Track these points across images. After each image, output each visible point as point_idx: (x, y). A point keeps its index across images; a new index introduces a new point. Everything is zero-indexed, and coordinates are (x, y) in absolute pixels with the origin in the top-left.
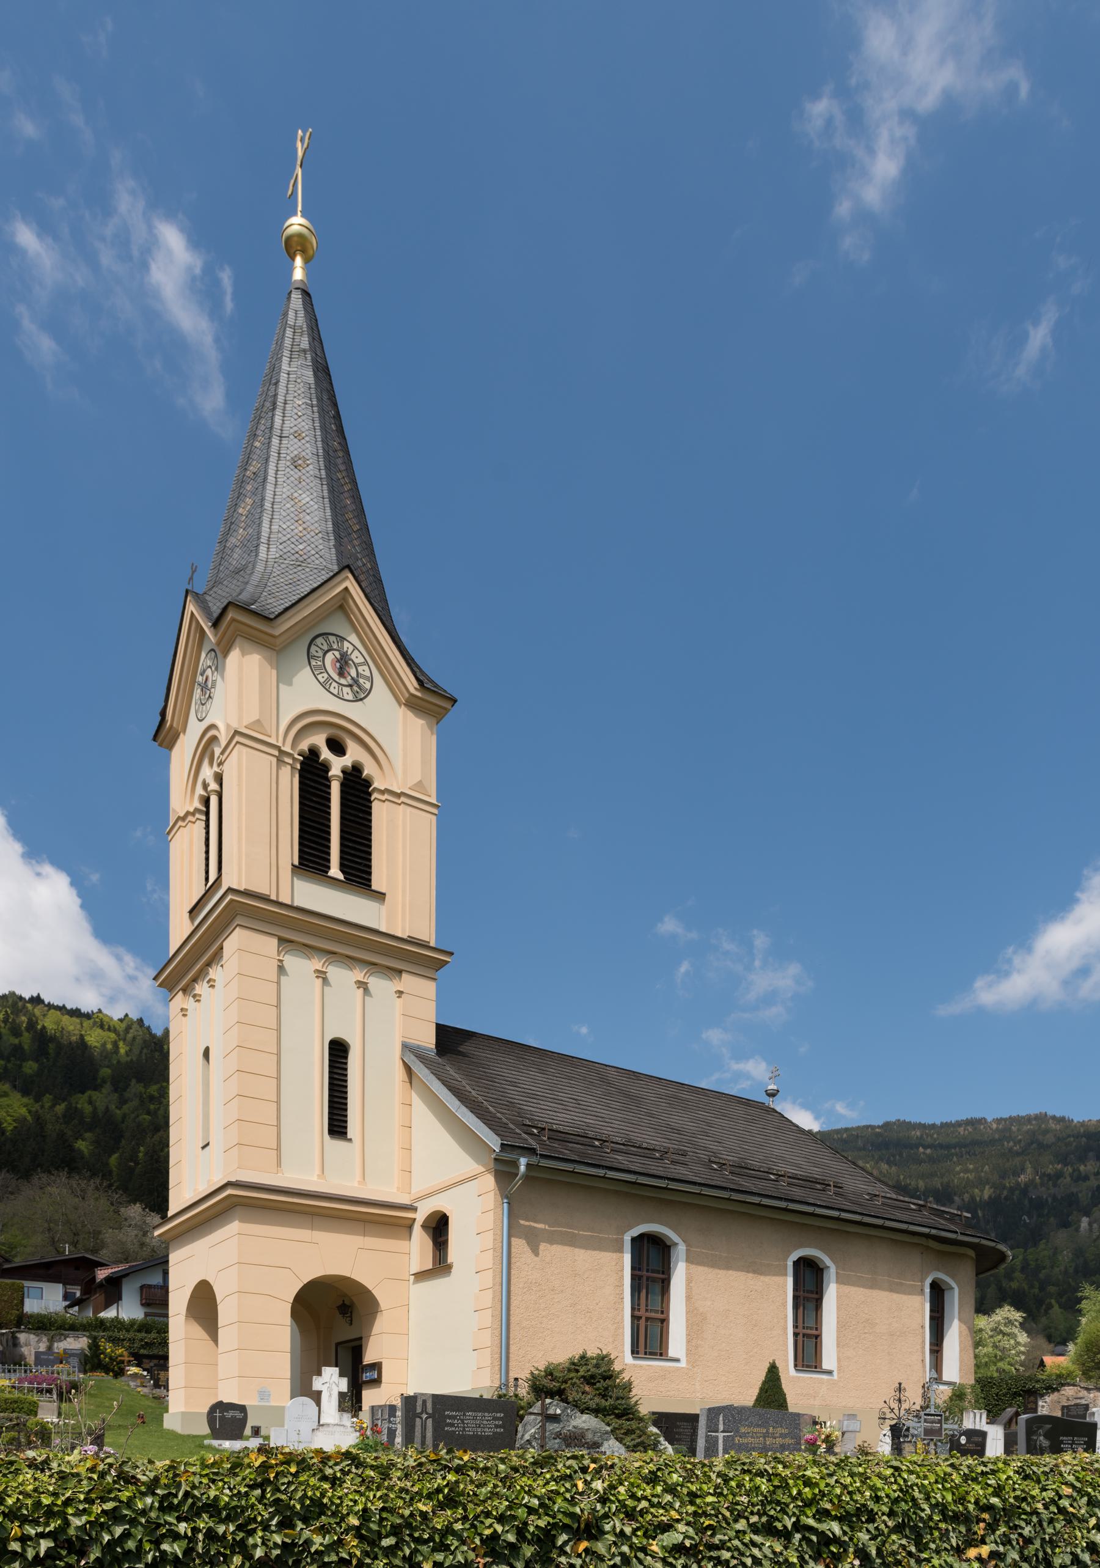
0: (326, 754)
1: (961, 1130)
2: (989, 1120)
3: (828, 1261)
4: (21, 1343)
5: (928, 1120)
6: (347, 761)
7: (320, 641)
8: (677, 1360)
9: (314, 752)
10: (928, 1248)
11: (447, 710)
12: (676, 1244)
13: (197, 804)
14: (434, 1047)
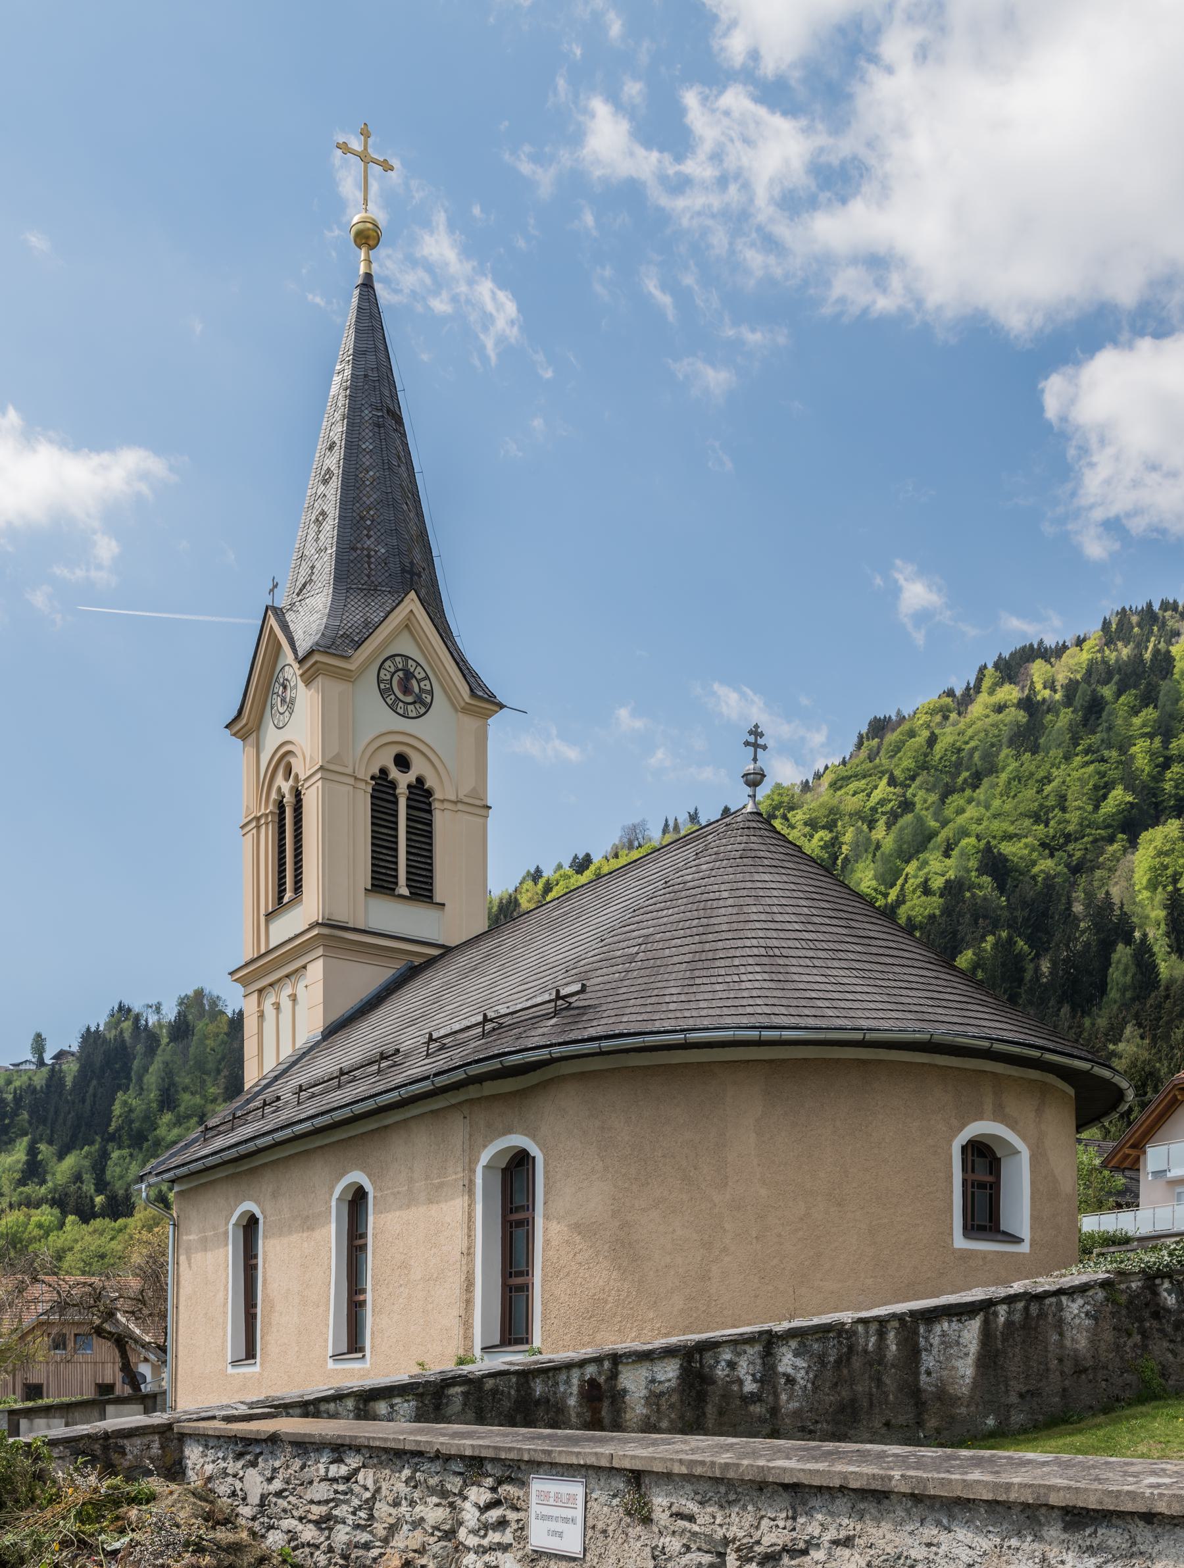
0: (394, 773)
6: (411, 777)
7: (388, 663)
9: (384, 771)
11: (497, 712)
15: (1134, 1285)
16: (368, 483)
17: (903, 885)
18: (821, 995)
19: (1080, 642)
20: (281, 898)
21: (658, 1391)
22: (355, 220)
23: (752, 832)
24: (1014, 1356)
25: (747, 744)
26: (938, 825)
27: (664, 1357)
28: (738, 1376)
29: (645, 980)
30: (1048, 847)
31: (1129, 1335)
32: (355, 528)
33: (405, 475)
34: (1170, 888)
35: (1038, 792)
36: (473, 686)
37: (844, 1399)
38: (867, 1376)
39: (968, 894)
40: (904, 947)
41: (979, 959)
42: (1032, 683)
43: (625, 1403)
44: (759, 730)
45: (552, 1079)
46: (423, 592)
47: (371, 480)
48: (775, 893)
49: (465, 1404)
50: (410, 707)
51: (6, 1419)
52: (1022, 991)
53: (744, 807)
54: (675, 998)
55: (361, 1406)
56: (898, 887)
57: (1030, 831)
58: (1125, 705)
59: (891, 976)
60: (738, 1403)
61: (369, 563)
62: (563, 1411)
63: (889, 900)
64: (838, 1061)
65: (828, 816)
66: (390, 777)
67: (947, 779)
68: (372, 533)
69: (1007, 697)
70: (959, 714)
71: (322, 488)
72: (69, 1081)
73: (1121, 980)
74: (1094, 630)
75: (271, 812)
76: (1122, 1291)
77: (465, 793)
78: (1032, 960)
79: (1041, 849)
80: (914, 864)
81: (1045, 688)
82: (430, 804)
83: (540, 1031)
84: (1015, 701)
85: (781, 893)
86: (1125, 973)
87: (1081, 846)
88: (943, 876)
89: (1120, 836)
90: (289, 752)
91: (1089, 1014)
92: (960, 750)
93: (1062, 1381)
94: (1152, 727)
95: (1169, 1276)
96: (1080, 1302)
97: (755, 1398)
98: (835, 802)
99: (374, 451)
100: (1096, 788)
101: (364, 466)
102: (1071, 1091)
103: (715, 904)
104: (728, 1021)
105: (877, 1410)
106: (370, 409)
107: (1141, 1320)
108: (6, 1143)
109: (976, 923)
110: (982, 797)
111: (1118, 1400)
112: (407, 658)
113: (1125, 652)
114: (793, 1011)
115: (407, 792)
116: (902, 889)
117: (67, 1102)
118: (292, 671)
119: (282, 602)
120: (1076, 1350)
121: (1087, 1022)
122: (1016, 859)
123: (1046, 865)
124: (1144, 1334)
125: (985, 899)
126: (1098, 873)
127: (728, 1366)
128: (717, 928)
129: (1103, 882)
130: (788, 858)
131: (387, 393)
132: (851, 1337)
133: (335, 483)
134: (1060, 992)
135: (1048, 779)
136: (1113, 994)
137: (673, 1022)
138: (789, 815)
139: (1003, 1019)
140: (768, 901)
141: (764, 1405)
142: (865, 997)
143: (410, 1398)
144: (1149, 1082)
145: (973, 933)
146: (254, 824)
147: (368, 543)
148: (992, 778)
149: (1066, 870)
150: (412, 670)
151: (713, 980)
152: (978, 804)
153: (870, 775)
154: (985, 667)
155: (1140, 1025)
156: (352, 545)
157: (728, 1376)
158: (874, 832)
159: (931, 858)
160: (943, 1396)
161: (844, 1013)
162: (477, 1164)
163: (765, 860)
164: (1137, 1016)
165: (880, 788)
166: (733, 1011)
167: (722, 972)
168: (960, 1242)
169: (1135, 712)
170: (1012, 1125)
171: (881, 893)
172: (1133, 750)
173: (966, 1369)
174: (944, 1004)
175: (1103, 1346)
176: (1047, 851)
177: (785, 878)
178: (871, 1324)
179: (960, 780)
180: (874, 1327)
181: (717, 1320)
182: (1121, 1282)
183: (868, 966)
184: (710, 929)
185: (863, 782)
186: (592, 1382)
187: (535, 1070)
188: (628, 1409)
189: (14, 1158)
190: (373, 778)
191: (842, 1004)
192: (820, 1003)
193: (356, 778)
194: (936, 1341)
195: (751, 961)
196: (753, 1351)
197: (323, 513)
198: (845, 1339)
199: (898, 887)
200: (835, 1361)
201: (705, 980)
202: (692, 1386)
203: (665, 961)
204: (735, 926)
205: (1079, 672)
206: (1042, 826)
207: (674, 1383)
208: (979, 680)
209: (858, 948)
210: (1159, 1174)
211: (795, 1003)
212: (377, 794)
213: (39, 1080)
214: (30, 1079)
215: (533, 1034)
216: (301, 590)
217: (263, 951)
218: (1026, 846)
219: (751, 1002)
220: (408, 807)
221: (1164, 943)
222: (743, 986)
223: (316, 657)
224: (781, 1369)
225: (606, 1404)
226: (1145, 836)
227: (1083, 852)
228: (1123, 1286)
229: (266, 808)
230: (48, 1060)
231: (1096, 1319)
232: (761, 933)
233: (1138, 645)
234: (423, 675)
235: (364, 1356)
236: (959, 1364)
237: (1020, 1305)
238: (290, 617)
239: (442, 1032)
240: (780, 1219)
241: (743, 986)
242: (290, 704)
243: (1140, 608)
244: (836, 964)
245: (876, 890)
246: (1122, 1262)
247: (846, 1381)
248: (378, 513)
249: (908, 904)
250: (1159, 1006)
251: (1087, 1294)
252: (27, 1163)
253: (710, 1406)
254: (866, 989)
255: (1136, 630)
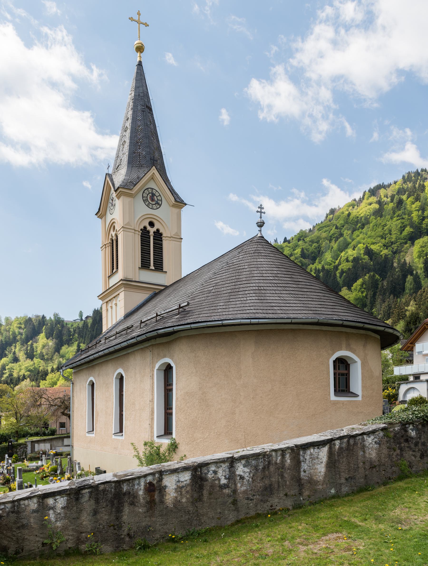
0: (149, 228)
6: (155, 229)
7: (146, 191)
9: (145, 228)
11: (184, 206)
13: (110, 241)
15: (396, 429)
16: (139, 131)
17: (340, 259)
18: (276, 305)
19: (395, 183)
20: (113, 271)
21: (181, 486)
22: (136, 43)
23: (259, 243)
24: (343, 462)
25: (258, 212)
26: (351, 240)
27: (184, 471)
28: (218, 477)
29: (213, 300)
30: (386, 246)
31: (395, 450)
32: (135, 146)
33: (153, 128)
34: (425, 258)
35: (382, 229)
36: (176, 198)
37: (266, 484)
38: (277, 474)
39: (360, 261)
40: (312, 284)
41: (364, 281)
42: (380, 196)
43: (165, 492)
44: (262, 207)
45: (178, 338)
46: (158, 167)
47: (140, 129)
48: (265, 266)
49: (90, 497)
50: (154, 206)
51: (30, 444)
52: (378, 291)
53: (257, 235)
54: (221, 307)
55: (41, 501)
56: (338, 260)
57: (380, 241)
58: (410, 201)
59: (306, 296)
60: (218, 489)
61: (140, 158)
62: (136, 497)
63: (336, 264)
64: (283, 330)
65: (316, 239)
66: (147, 229)
67: (353, 226)
68: (141, 147)
69: (373, 200)
70: (358, 206)
71: (124, 133)
72: (89, 325)
73: (410, 287)
74: (399, 178)
75: (109, 243)
76: (391, 432)
77: (173, 234)
78: (381, 281)
79: (383, 247)
80: (344, 253)
81: (384, 197)
82: (161, 238)
83: (172, 320)
84: (375, 202)
85: (267, 266)
86: (411, 284)
87: (396, 246)
88: (353, 256)
89: (409, 242)
90: (114, 222)
91: (399, 298)
92: (358, 217)
93: (365, 472)
94: (419, 208)
95: (412, 423)
96: (372, 437)
97: (226, 486)
98: (319, 235)
99: (142, 120)
100: (401, 227)
101: (138, 125)
102: (379, 337)
103: (242, 270)
104: (239, 316)
105: (281, 489)
106: (140, 106)
107: (400, 443)
108: (71, 344)
109: (363, 270)
110: (365, 231)
111: (390, 479)
112: (153, 189)
113: (410, 185)
114: (264, 311)
115: (153, 234)
116: (340, 261)
117: (89, 331)
118: (114, 195)
119: (110, 172)
120: (371, 458)
121: (399, 300)
122: (376, 250)
123: (385, 252)
124: (401, 449)
125: (366, 263)
126: (402, 254)
127: (213, 473)
128: (241, 280)
129: (404, 256)
130: (271, 252)
131: (146, 100)
132: (269, 457)
133: (129, 131)
134: (390, 291)
135: (385, 225)
136: (407, 291)
137: (218, 317)
138: (305, 239)
139: (349, 312)
140: (262, 269)
141: (230, 489)
142: (294, 305)
143: (64, 496)
144: (417, 320)
145: (362, 273)
146: (104, 247)
147: (139, 151)
148: (368, 225)
149: (391, 253)
150: (154, 193)
151: (237, 299)
152: (364, 234)
153: (330, 226)
154: (366, 191)
155: (415, 301)
156: (134, 152)
157: (213, 477)
158: (331, 243)
159: (349, 251)
160: (311, 481)
161: (284, 312)
162: (155, 368)
163: (262, 254)
164: (414, 298)
165: (333, 230)
166: (241, 312)
167: (241, 296)
168: (333, 398)
169: (413, 203)
170: (354, 352)
171: (333, 262)
172: (412, 215)
173: (321, 469)
174: (326, 306)
175: (383, 456)
176: (385, 247)
177: (269, 260)
178: (278, 452)
179: (358, 226)
180: (279, 453)
181: (238, 430)
182: (391, 428)
183: (297, 293)
184: (239, 280)
185: (328, 228)
186: (150, 484)
187: (173, 334)
188: (167, 495)
189: (73, 348)
190: (141, 230)
191: (284, 308)
192: (275, 308)
193: (135, 230)
194: (308, 457)
195: (252, 292)
196: (225, 466)
197: (125, 142)
198: (267, 458)
199: (338, 260)
200: (262, 468)
201: (233, 300)
202: (196, 482)
203: (221, 293)
204: (248, 279)
205: (395, 192)
206: (384, 240)
207: (188, 482)
208: (364, 196)
209: (294, 286)
210: (420, 353)
211: (266, 308)
212: (143, 235)
213: (81, 325)
214: (78, 324)
215: (169, 322)
216: (117, 168)
217: (107, 288)
218: (379, 246)
219: (249, 308)
220: (154, 239)
221: (423, 274)
222: (248, 302)
223: (120, 190)
224: (237, 473)
225: (157, 493)
226: (416, 242)
227: (397, 247)
228: (391, 429)
229: (108, 242)
230: (84, 319)
231: (379, 444)
232: (257, 281)
233: (414, 183)
234: (158, 194)
235: (122, 435)
236: (318, 467)
237: (345, 440)
238: (114, 177)
239: (145, 320)
240: (261, 391)
241: (248, 302)
242: (114, 205)
243: (414, 171)
244: (284, 292)
245: (332, 261)
246: (391, 418)
247: (267, 477)
248: (143, 141)
249: (342, 265)
250: (422, 295)
251: (375, 434)
252: (77, 349)
253: (205, 491)
254: (295, 302)
255: (413, 178)
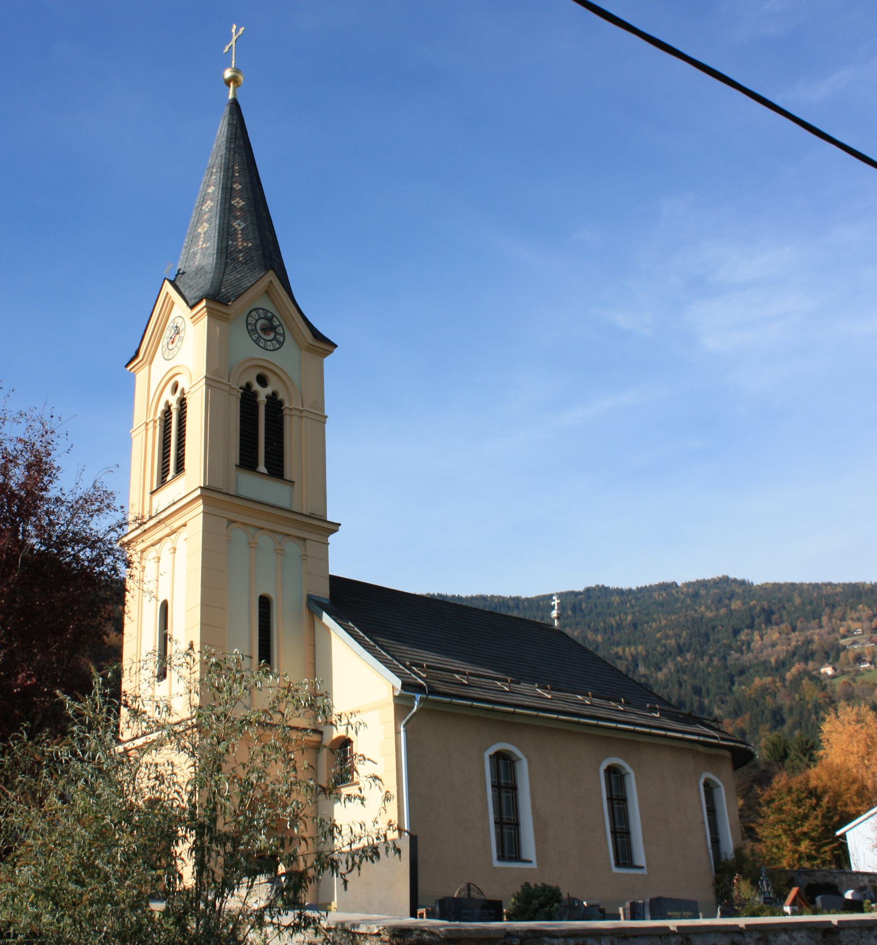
0: (256, 387)
1: (656, 595)
2: (679, 584)
3: (628, 769)
4: (780, 938)
5: (625, 585)
6: (268, 391)
7: (254, 313)
8: (530, 862)
9: (249, 386)
10: (698, 753)
12: (520, 759)
14: (328, 597)
50: (269, 343)
168: (496, 864)
